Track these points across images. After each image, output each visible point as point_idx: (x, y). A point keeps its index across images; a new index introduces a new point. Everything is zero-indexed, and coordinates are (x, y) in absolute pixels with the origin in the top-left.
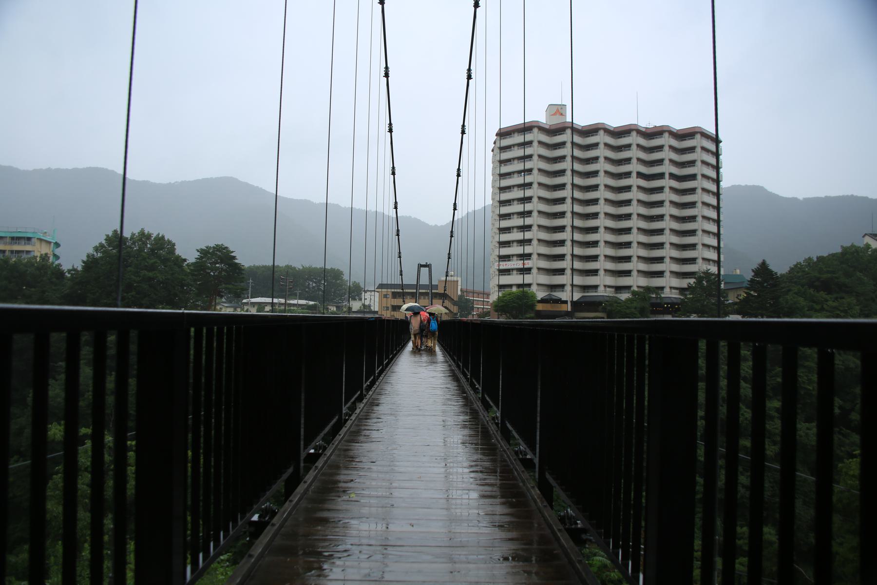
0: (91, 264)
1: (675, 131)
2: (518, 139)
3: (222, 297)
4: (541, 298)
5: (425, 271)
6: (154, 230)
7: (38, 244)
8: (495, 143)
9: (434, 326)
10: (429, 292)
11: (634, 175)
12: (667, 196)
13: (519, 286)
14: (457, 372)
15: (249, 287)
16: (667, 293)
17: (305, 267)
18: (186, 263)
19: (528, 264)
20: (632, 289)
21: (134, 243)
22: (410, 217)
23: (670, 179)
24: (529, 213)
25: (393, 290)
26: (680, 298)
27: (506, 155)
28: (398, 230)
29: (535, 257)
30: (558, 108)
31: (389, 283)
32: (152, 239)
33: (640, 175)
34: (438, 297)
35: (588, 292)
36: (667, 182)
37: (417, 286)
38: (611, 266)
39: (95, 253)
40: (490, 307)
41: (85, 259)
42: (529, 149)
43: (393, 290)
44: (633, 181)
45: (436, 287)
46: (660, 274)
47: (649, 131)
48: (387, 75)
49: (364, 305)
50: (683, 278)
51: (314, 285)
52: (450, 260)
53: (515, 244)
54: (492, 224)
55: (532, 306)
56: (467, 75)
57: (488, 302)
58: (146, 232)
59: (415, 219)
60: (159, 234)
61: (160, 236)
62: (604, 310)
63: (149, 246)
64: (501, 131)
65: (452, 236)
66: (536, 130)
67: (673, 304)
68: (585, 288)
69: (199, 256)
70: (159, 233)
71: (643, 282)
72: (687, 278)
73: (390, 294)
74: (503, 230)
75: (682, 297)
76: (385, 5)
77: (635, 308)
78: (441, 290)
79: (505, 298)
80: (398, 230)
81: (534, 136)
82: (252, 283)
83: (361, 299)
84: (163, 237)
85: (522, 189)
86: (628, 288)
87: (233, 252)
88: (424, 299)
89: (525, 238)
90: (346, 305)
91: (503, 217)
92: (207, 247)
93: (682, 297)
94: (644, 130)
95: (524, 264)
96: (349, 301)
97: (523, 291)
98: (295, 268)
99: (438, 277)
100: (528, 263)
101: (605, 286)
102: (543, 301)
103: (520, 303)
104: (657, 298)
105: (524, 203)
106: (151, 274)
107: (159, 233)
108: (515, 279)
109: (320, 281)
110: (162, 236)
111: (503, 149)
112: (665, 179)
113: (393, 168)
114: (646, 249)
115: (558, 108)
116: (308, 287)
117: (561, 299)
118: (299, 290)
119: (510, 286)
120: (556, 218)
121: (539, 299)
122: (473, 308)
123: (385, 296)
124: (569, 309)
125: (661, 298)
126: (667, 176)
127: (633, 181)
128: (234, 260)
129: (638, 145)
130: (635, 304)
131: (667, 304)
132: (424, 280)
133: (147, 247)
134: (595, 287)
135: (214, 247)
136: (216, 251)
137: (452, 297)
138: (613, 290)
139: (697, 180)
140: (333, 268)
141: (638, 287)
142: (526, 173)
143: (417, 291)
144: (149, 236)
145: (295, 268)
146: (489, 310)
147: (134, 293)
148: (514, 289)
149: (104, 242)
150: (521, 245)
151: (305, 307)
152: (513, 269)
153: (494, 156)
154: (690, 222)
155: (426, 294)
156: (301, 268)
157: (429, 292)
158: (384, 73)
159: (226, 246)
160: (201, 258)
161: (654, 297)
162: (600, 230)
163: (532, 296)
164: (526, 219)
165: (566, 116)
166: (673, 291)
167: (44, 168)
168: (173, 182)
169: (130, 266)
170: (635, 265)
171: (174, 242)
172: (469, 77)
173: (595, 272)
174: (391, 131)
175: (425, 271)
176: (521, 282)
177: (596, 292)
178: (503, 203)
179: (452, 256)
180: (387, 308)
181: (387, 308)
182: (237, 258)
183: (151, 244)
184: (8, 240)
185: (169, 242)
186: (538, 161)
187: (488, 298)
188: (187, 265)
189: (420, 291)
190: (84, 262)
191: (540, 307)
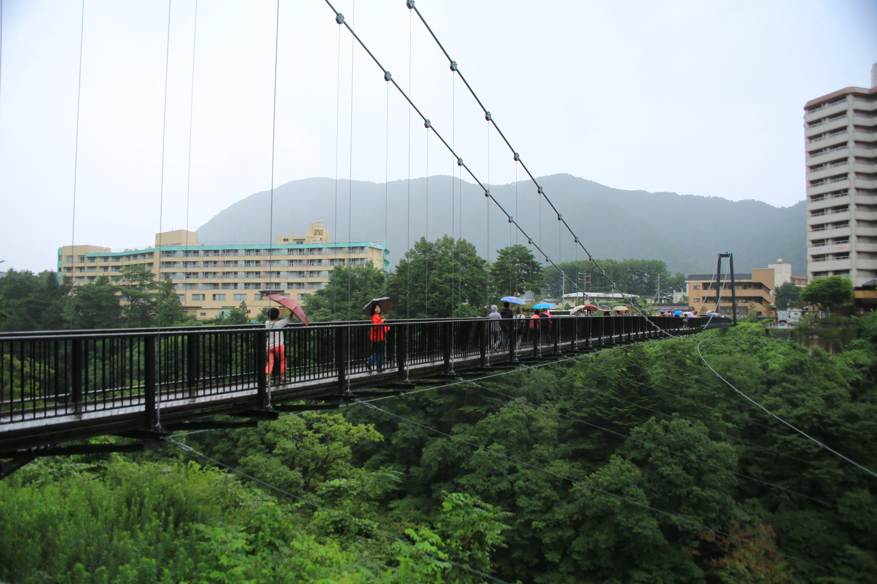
0: (403, 269)
5: (725, 261)
7: (370, 251)
15: (562, 284)
21: (439, 248)
22: (753, 200)
39: (406, 259)
41: (398, 264)
49: (684, 297)
51: (637, 278)
59: (759, 202)
73: (701, 285)
81: (851, 104)
84: (465, 241)
87: (530, 251)
96: (672, 292)
100: (845, 247)
102: (865, 288)
106: (452, 276)
109: (642, 274)
116: (631, 280)
119: (826, 272)
135: (512, 248)
145: (616, 262)
147: (437, 293)
149: (414, 248)
152: (828, 255)
160: (502, 258)
163: (846, 283)
167: (395, 180)
169: (435, 269)
181: (698, 300)
184: (347, 250)
185: (470, 245)
190: (397, 267)
191: (860, 295)
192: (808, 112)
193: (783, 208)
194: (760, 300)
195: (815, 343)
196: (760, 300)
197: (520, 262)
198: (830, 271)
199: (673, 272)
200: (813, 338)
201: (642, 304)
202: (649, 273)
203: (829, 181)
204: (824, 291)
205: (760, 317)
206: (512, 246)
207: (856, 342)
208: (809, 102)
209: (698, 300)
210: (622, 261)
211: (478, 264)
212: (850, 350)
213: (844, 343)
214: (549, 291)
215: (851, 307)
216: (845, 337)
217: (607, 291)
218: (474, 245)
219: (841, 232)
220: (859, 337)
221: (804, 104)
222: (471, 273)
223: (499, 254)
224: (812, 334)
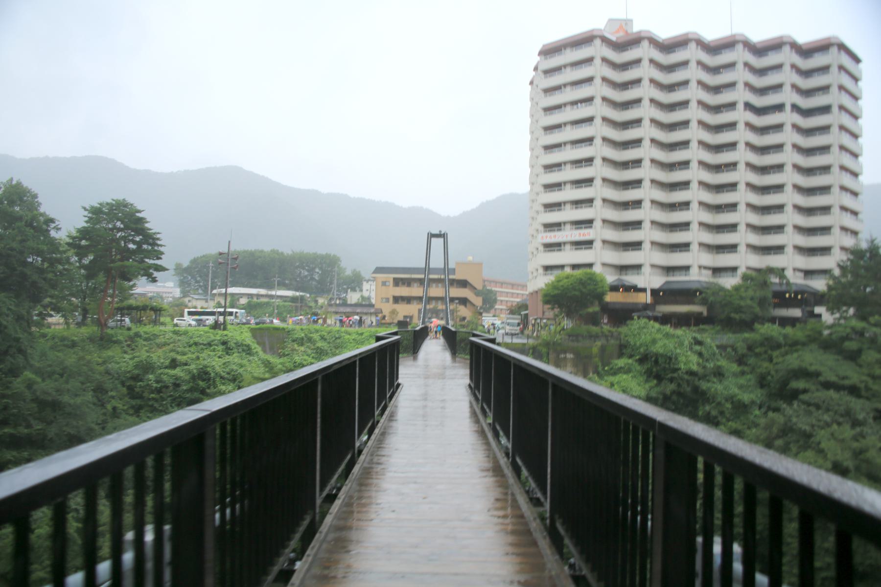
17: (295, 252)
34: (455, 285)
36: (788, 117)
37: (427, 269)
45: (453, 271)
49: (363, 297)
51: (306, 273)
53: (568, 206)
55: (600, 297)
60: (12, 180)
61: (14, 182)
62: (704, 302)
68: (669, 270)
73: (392, 281)
77: (752, 299)
79: (561, 284)
81: (597, 50)
82: (213, 267)
83: (361, 290)
88: (437, 286)
92: (100, 204)
96: (347, 292)
102: (614, 288)
103: (584, 290)
104: (781, 284)
109: (314, 269)
110: (17, 182)
117: (637, 286)
118: (278, 277)
119: (562, 267)
122: (495, 301)
123: (384, 284)
124: (649, 300)
126: (788, 108)
130: (750, 293)
132: (437, 262)
134: (686, 268)
143: (425, 276)
145: (282, 253)
148: (568, 270)
151: (289, 299)
173: (636, 245)
175: (437, 243)
180: (387, 300)
189: (431, 276)
191: (610, 298)
192: (543, 57)
193: (448, 217)
194: (464, 301)
195: (569, 364)
196: (464, 301)
197: (127, 228)
198: (568, 265)
199: (348, 266)
200: (565, 358)
201: (312, 304)
202: (321, 269)
203: (568, 146)
204: (575, 290)
206: (110, 201)
207: (621, 362)
208: (544, 46)
209: (387, 300)
210: (290, 253)
212: (614, 374)
213: (604, 366)
214: (200, 286)
215: (595, 313)
216: (605, 356)
217: (270, 287)
219: (583, 213)
220: (621, 355)
221: (539, 48)
222: (19, 238)
223: (86, 213)
224: (565, 352)
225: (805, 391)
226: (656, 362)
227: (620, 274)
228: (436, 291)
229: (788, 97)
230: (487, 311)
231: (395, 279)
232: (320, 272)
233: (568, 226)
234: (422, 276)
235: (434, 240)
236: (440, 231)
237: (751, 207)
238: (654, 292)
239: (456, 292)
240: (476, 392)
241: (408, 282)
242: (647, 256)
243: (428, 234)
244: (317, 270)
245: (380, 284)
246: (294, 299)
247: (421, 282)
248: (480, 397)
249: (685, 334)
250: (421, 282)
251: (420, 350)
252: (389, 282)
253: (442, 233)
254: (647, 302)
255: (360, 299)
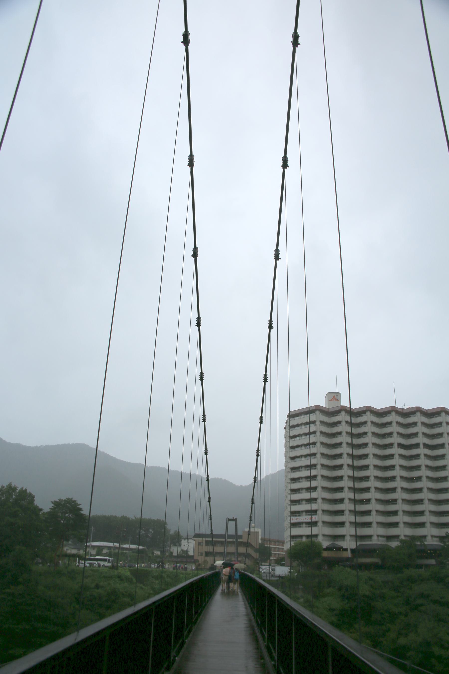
1: (425, 411)
2: (304, 419)
3: (68, 540)
4: (326, 547)
6: (19, 485)
8: (286, 422)
9: (237, 576)
10: (235, 541)
11: (396, 446)
12: (423, 461)
13: (308, 536)
14: (256, 628)
16: (429, 541)
17: (136, 517)
18: (42, 512)
19: (315, 518)
20: (400, 538)
22: (221, 479)
23: (424, 448)
24: (315, 489)
25: (207, 539)
26: (440, 545)
27: (296, 442)
28: (209, 498)
29: (320, 512)
30: (334, 396)
31: (204, 533)
32: (17, 491)
33: (400, 446)
35: (364, 541)
36: (422, 451)
38: (381, 519)
40: (285, 553)
42: (314, 459)
43: (207, 539)
44: (395, 450)
45: (241, 537)
46: (422, 525)
47: (405, 412)
48: (202, 379)
50: (442, 528)
52: (259, 457)
53: (304, 491)
54: (284, 480)
55: (319, 554)
56: (263, 378)
57: (283, 549)
58: (13, 485)
60: (23, 488)
61: (24, 489)
63: (14, 497)
64: (290, 414)
65: (253, 503)
66: (318, 412)
67: (435, 550)
69: (52, 506)
70: (23, 487)
71: (409, 532)
72: (444, 528)
73: (204, 542)
74: (294, 491)
75: (442, 544)
76: (201, 327)
78: (244, 540)
80: (209, 498)
83: (180, 545)
85: (309, 469)
86: (397, 537)
87: (80, 505)
89: (312, 497)
90: (168, 550)
91: (294, 480)
92: (60, 500)
93: (442, 544)
94: (401, 411)
95: (311, 518)
96: (170, 546)
97: (312, 542)
98: (129, 518)
99: (243, 528)
100: (315, 518)
101: (378, 536)
102: (328, 549)
105: (311, 527)
107: (23, 487)
108: (305, 531)
110: (25, 489)
111: (292, 427)
112: (420, 448)
113: (206, 449)
114: (407, 482)
115: (334, 396)
117: (342, 547)
119: (301, 536)
120: (336, 481)
121: (324, 547)
122: (270, 554)
125: (425, 545)
126: (421, 446)
127: (395, 450)
128: (81, 511)
129: (397, 423)
131: (430, 550)
132: (231, 531)
133: (12, 498)
134: (370, 537)
135: (65, 500)
136: (67, 504)
137: (253, 544)
138: (384, 539)
139: (445, 448)
140: (159, 519)
141: (405, 536)
142: (311, 446)
144: (14, 489)
146: (284, 556)
148: (304, 539)
150: (308, 503)
152: (302, 523)
153: (286, 433)
154: (443, 482)
155: (233, 542)
156: (134, 518)
157: (235, 541)
158: (200, 377)
159: (74, 500)
160: (54, 509)
161: (418, 545)
162: (369, 456)
164: (313, 516)
165: (340, 401)
166: (434, 539)
168: (39, 446)
170: (401, 518)
171: (33, 495)
172: (266, 380)
174: (204, 421)
175: (232, 524)
176: (310, 533)
177: (371, 541)
178: (293, 469)
179: (255, 501)
181: (202, 554)
182: (83, 509)
183: (16, 496)
186: (346, 436)
187: (283, 546)
188: (43, 514)
189: (229, 540)
191: (325, 554)
199: (172, 528)
205: (199, 567)
209: (202, 554)
211: (37, 510)
218: (34, 494)
223: (53, 505)
225: (422, 605)
226: (347, 590)
227: (334, 541)
228: (231, 549)
229: (421, 440)
230: (264, 561)
231: (206, 541)
232: (153, 532)
233: (304, 513)
234: (223, 540)
235: (229, 522)
236: (233, 518)
237: (430, 489)
238: (353, 551)
239: (242, 550)
240: (263, 630)
241: (213, 544)
242: (348, 530)
243: (227, 519)
244: (151, 530)
245: (198, 544)
246: (139, 551)
247: (222, 543)
248: (266, 636)
249: (365, 574)
250: (222, 543)
251: (325, 534)
252: (203, 543)
253: (234, 518)
254: (349, 556)
255: (181, 552)
